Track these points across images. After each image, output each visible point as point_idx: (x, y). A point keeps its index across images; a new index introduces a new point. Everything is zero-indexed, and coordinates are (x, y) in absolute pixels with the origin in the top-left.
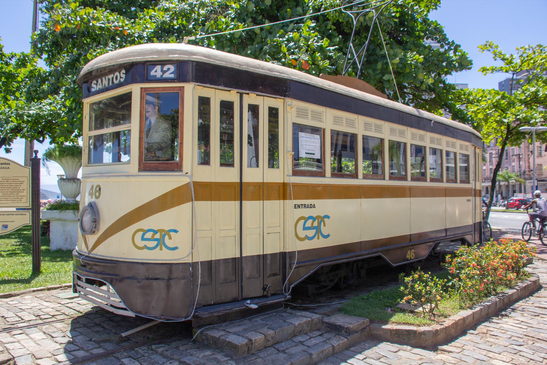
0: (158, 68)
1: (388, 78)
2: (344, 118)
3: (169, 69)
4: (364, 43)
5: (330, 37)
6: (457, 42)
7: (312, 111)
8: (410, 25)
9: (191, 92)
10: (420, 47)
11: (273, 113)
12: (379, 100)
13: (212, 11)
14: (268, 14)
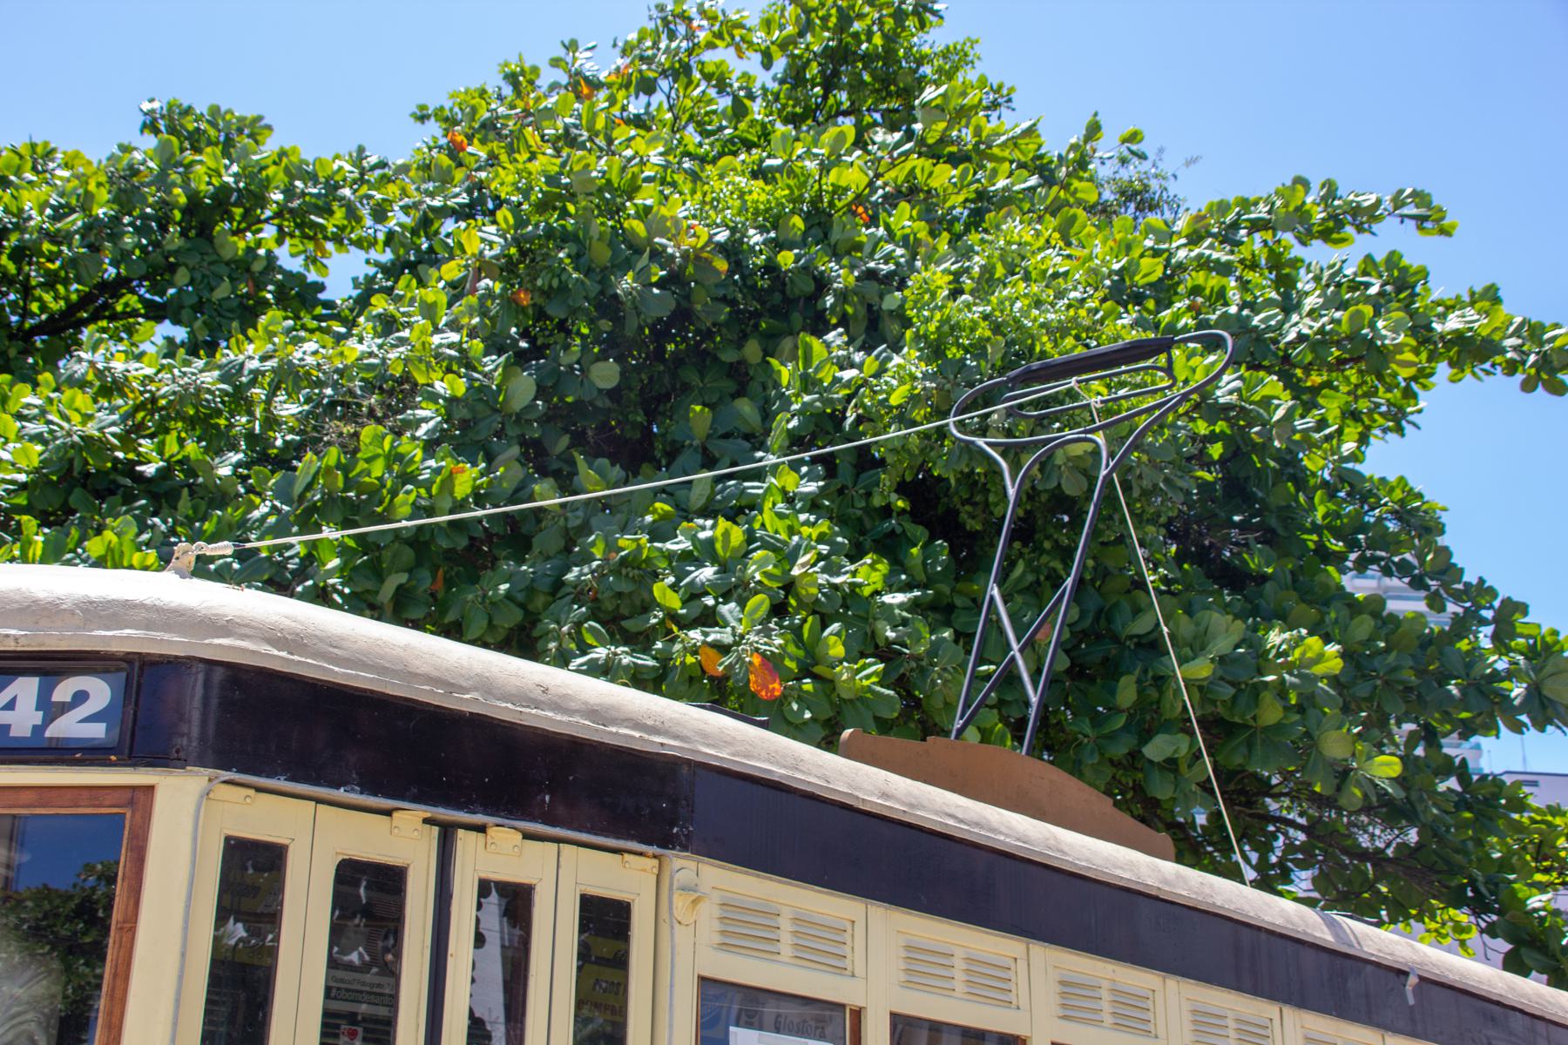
0: (26, 688)
1: (1168, 752)
2: (959, 954)
3: (81, 697)
4: (1057, 582)
5: (891, 548)
6: (1506, 589)
7: (796, 920)
8: (1275, 500)
9: (189, 817)
10: (1327, 603)
11: (604, 922)
12: (1131, 865)
13: (333, 404)
14: (604, 427)
